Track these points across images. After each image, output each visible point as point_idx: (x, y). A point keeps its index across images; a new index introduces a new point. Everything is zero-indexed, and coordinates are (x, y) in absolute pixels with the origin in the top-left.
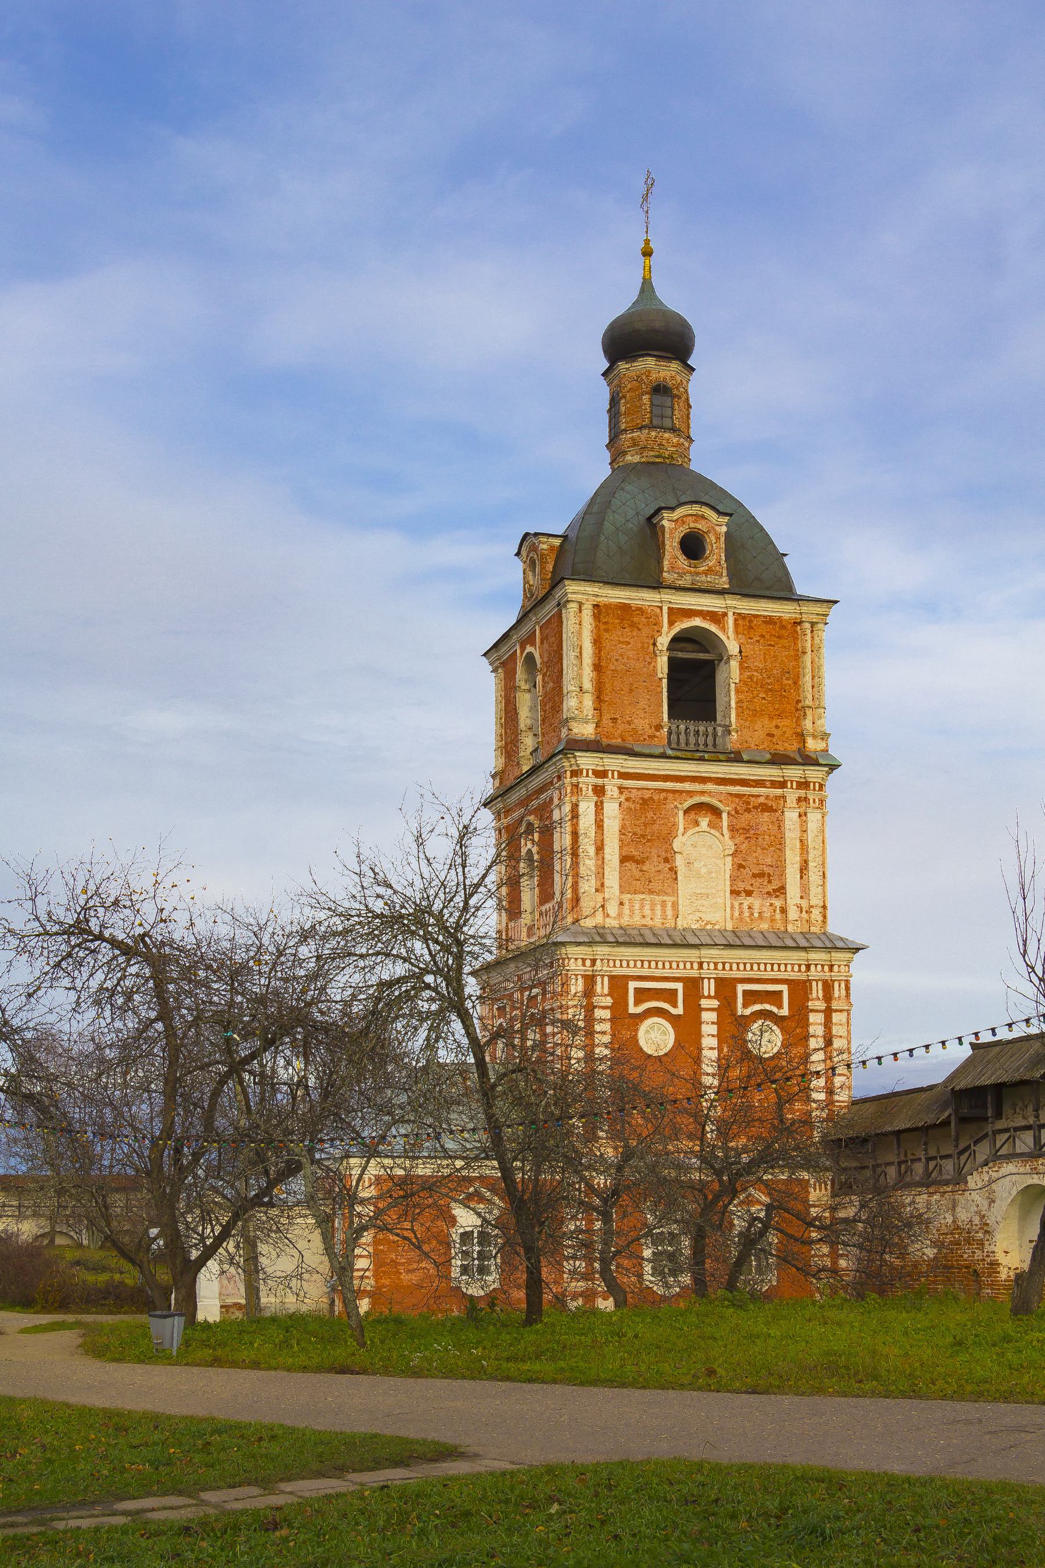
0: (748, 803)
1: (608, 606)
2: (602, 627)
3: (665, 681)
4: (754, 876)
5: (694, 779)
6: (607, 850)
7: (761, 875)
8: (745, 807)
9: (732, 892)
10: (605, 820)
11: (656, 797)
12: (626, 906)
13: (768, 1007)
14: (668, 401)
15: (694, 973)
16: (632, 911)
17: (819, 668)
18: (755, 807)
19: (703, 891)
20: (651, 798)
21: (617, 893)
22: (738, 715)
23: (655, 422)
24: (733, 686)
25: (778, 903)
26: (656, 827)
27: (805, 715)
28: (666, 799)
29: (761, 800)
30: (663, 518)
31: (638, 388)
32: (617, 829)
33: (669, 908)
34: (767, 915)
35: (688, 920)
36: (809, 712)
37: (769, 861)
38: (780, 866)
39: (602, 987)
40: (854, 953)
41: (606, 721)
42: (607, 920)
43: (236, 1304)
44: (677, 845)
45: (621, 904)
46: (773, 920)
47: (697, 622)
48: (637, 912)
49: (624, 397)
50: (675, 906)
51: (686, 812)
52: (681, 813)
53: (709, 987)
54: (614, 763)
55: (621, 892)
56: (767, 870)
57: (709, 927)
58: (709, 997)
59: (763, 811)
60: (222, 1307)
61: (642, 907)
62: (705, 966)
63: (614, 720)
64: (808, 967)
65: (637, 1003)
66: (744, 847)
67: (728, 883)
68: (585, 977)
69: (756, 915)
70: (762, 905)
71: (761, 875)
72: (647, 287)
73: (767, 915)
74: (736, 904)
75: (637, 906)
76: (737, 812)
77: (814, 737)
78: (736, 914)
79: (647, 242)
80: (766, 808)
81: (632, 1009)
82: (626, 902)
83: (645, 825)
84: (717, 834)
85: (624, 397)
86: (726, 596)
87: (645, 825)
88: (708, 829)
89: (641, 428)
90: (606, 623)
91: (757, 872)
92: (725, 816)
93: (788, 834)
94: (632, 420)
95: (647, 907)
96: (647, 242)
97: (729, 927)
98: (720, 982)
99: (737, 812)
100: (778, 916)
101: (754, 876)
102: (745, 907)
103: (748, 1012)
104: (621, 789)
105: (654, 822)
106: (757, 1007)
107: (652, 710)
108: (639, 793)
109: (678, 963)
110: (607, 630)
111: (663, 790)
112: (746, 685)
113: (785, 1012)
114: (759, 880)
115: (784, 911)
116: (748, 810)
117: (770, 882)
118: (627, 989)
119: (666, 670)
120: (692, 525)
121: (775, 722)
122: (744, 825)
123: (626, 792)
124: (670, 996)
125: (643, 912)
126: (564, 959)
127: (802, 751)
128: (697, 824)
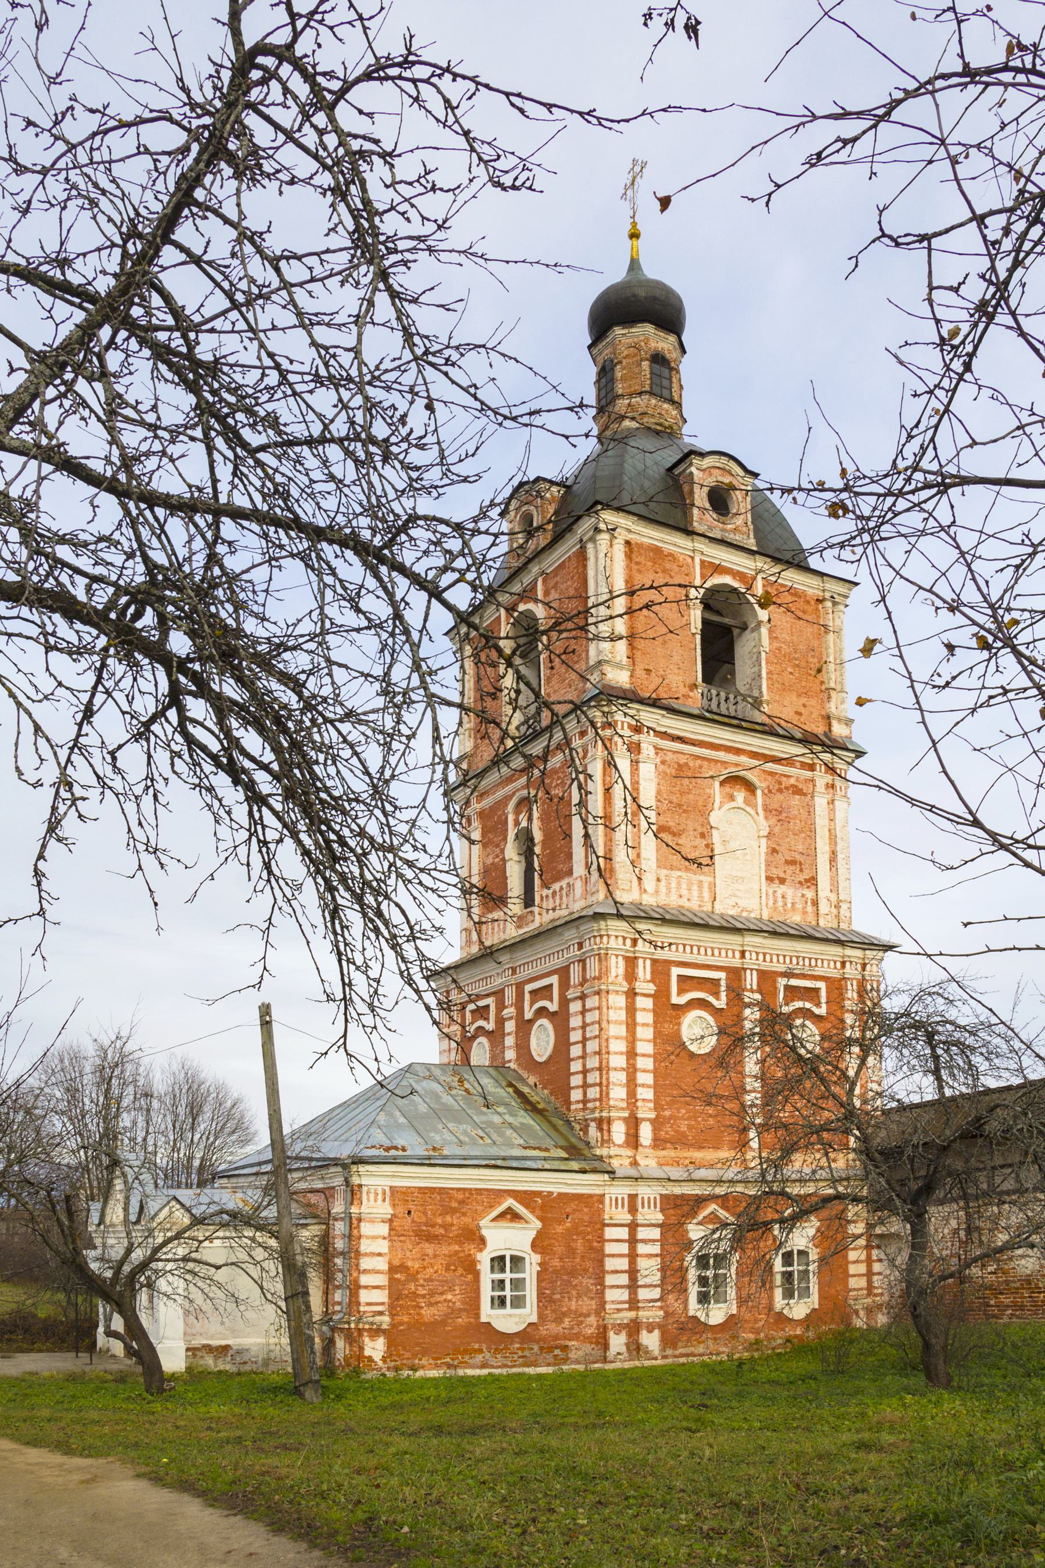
0: (780, 783)
1: (640, 546)
2: (635, 567)
3: (698, 637)
4: (787, 862)
5: (728, 749)
6: (827, 856)
7: (792, 862)
8: (777, 786)
9: (770, 879)
10: (641, 782)
11: (691, 764)
12: (663, 883)
13: (808, 1005)
14: (665, 372)
15: (736, 962)
16: (669, 889)
17: (841, 651)
18: (787, 788)
19: (739, 874)
20: (686, 764)
21: (654, 865)
22: (768, 688)
23: (656, 390)
24: (763, 654)
25: (810, 894)
26: (691, 797)
27: (829, 697)
28: (701, 767)
29: (792, 781)
30: (691, 464)
31: (635, 355)
32: (653, 793)
33: (706, 889)
34: (799, 906)
35: (725, 907)
36: (833, 694)
37: (800, 847)
38: (812, 853)
39: (644, 970)
40: (885, 951)
41: (640, 672)
42: (644, 896)
43: (204, 1346)
44: (714, 818)
45: (658, 880)
46: (805, 913)
47: (728, 580)
48: (674, 890)
49: (620, 362)
50: (713, 886)
51: (722, 783)
52: (717, 784)
53: (751, 980)
54: (650, 717)
55: (658, 867)
56: (798, 857)
57: (745, 914)
58: (752, 991)
59: (794, 793)
60: (188, 1350)
61: (679, 884)
62: (747, 954)
63: (648, 671)
64: (843, 964)
65: (681, 992)
66: (777, 830)
67: (763, 867)
68: (627, 959)
69: (789, 905)
70: (794, 896)
71: (792, 862)
72: (634, 265)
73: (799, 906)
74: (771, 892)
75: (674, 885)
76: (770, 791)
77: (839, 720)
78: (771, 902)
79: (634, 224)
80: (798, 791)
81: (675, 999)
82: (662, 878)
83: (682, 793)
84: (752, 812)
85: (620, 362)
86: (757, 557)
87: (682, 793)
88: (743, 806)
89: (641, 393)
90: (638, 563)
91: (792, 861)
92: (759, 792)
93: (818, 821)
94: (630, 386)
95: (684, 886)
96: (634, 224)
97: (765, 917)
98: (763, 974)
99: (770, 791)
100: (810, 908)
101: (787, 862)
102: (779, 895)
103: (682, 1000)
104: (658, 749)
105: (689, 792)
106: (799, 1004)
107: (681, 667)
108: (675, 756)
109: (718, 952)
110: (640, 571)
111: (699, 757)
112: (776, 656)
113: (822, 1011)
114: (792, 868)
115: (815, 903)
116: (780, 791)
117: (801, 870)
118: (669, 976)
119: (699, 626)
120: (720, 479)
121: (803, 700)
122: (776, 806)
123: (661, 754)
124: (712, 986)
125: (680, 891)
126: (601, 936)
127: (828, 733)
128: (732, 798)
